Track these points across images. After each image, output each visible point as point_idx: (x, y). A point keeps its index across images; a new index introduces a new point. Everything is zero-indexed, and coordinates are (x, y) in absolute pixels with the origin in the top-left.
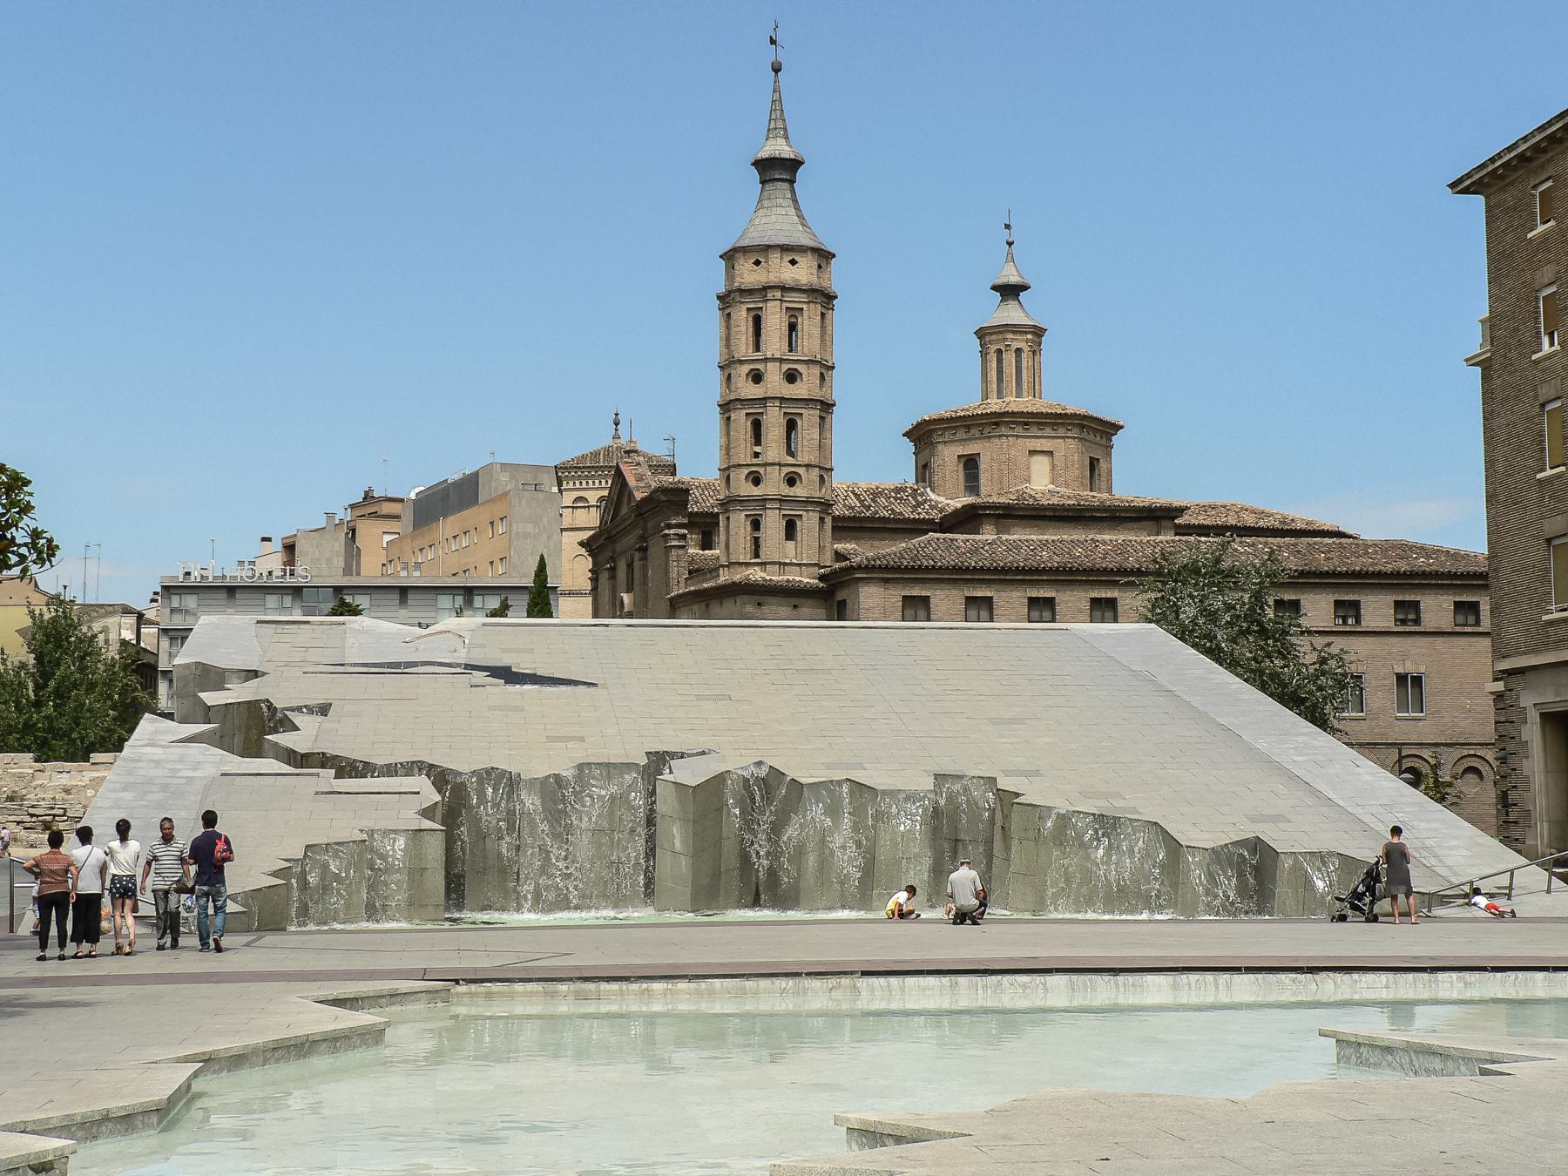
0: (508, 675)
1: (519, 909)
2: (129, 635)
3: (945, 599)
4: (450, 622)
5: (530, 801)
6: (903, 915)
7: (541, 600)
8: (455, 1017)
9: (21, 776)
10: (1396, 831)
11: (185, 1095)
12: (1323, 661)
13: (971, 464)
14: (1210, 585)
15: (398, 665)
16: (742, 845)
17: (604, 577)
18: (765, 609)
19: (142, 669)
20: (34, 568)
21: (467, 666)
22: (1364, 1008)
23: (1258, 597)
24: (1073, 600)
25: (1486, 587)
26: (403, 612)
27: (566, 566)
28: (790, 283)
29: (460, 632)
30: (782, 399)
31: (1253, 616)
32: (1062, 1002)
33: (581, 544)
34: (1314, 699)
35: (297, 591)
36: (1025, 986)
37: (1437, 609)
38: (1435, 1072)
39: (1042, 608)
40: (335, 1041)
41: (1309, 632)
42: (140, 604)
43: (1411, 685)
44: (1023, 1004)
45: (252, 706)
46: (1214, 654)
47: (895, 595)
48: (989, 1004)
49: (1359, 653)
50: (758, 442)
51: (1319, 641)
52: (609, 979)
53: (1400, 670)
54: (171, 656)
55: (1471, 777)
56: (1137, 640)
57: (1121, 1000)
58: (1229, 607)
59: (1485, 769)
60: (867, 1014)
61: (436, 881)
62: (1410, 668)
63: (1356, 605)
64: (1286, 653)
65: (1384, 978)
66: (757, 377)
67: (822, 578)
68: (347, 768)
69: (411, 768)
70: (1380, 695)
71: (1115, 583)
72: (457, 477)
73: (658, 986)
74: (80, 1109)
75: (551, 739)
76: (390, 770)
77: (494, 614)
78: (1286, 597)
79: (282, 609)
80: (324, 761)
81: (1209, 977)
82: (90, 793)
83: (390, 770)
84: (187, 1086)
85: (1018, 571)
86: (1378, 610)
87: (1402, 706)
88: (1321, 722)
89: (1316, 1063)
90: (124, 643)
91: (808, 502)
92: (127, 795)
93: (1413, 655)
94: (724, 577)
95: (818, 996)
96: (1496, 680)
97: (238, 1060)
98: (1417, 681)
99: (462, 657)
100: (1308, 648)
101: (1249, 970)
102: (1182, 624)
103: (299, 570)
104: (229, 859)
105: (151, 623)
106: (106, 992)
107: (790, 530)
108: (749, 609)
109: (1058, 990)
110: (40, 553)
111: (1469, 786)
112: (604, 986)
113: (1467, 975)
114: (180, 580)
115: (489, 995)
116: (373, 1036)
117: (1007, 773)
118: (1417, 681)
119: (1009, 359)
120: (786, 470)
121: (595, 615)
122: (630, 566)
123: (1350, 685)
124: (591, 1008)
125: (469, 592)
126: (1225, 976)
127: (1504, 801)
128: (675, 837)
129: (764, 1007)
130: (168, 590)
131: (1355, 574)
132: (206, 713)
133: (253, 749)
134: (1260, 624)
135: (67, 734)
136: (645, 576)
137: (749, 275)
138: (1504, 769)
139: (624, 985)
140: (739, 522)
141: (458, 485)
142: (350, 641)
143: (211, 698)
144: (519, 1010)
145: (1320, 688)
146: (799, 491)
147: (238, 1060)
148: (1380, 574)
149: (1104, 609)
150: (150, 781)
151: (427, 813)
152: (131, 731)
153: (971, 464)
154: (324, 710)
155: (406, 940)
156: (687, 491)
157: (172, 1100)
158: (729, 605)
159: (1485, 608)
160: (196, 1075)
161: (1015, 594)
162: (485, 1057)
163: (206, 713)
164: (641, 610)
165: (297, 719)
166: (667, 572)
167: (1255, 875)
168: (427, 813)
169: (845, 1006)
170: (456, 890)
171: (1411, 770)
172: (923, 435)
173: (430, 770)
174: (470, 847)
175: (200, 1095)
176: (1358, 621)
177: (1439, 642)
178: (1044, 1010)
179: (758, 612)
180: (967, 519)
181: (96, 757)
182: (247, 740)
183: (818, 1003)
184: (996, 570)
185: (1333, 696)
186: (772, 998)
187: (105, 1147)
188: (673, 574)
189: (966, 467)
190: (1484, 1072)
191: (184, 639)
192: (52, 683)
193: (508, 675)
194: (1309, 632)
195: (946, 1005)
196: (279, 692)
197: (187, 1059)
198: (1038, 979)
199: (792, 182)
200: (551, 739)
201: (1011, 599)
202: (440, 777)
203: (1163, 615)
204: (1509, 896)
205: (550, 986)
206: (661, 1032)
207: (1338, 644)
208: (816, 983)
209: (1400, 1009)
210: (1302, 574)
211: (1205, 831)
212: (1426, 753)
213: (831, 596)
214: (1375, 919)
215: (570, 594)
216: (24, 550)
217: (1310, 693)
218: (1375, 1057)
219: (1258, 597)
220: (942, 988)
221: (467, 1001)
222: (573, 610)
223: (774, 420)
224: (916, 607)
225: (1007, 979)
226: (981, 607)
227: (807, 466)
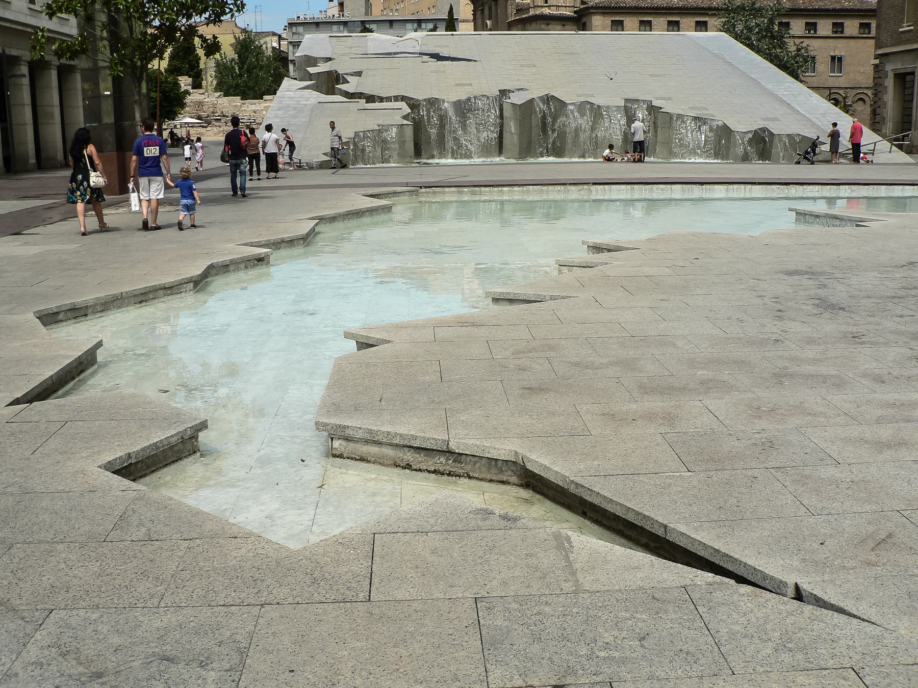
0: (437, 57)
1: (445, 157)
2: (275, 45)
3: (630, 22)
4: (413, 35)
6: (608, 159)
7: (451, 24)
8: (421, 202)
9: (236, 106)
10: (835, 125)
11: (312, 233)
12: (799, 50)
14: (750, 15)
15: (390, 54)
16: (539, 128)
17: (479, 13)
18: (550, 26)
19: (281, 59)
20: (236, 14)
21: (420, 54)
22: (815, 200)
23: (771, 21)
24: (687, 22)
25: (874, 16)
26: (391, 31)
27: (462, 8)
29: (416, 39)
31: (768, 29)
32: (678, 196)
34: (794, 66)
35: (345, 23)
36: (662, 190)
37: (851, 26)
38: (837, 226)
39: (674, 26)
40: (372, 211)
41: (794, 37)
42: (280, 31)
43: (837, 61)
44: (662, 197)
45: (329, 73)
46: (751, 46)
47: (608, 20)
48: (689, 197)
49: (815, 46)
51: (798, 41)
52: (485, 186)
53: (833, 54)
54: (294, 53)
55: (860, 103)
56: (716, 39)
57: (704, 196)
58: (758, 25)
59: (867, 99)
60: (594, 201)
61: (410, 146)
62: (837, 53)
63: (815, 24)
64: (782, 46)
65: (817, 187)
67: (575, 12)
68: (370, 99)
69: (396, 98)
70: (823, 66)
71: (707, 14)
73: (505, 189)
74: (273, 238)
75: (456, 85)
76: (389, 99)
77: (431, 30)
78: (784, 21)
79: (339, 31)
80: (360, 95)
81: (742, 186)
82: (264, 112)
83: (389, 99)
84: (313, 229)
85: (663, 8)
86: (825, 27)
87: (833, 71)
88: (796, 77)
89: (786, 222)
90: (273, 48)
92: (280, 112)
93: (839, 48)
94: (532, 12)
95: (574, 193)
96: (875, 58)
97: (333, 219)
98: (840, 59)
99: (418, 50)
100: (792, 44)
101: (760, 184)
102: (736, 33)
103: (346, 14)
104: (651, 102)
105: (284, 39)
106: (278, 192)
108: (543, 26)
109: (677, 191)
110: (238, 7)
111: (859, 107)
112: (483, 189)
113: (853, 187)
114: (296, 21)
115: (434, 193)
116: (387, 209)
117: (657, 99)
118: (840, 59)
121: (475, 30)
122: (490, 8)
123: (810, 61)
124: (477, 198)
125: (419, 22)
126: (749, 186)
127: (874, 113)
128: (512, 127)
129: (551, 197)
130: (291, 25)
131: (816, 10)
132: (310, 77)
133: (331, 91)
134: (771, 33)
135: (253, 88)
136: (497, 15)
138: (876, 99)
139: (491, 188)
142: (369, 44)
143: (312, 70)
144: (447, 199)
145: (797, 62)
147: (333, 219)
148: (827, 10)
149: (702, 26)
150: (288, 106)
152: (279, 86)
154: (359, 74)
155: (397, 171)
157: (308, 234)
158: (534, 25)
159: (874, 26)
160: (316, 224)
161: (662, 19)
162: (433, 218)
163: (310, 77)
164: (495, 28)
165: (349, 78)
166: (506, 10)
167: (762, 144)
168: (405, 117)
169: (585, 198)
170: (418, 153)
171: (833, 99)
173: (403, 98)
174: (426, 132)
175: (318, 233)
176: (815, 32)
177: (852, 42)
178: (671, 200)
179: (547, 28)
181: (266, 97)
182: (328, 88)
183: (573, 196)
184: (653, 8)
185: (802, 66)
186: (555, 194)
187: (284, 252)
188: (509, 12)
190: (857, 226)
191: (299, 46)
192: (245, 67)
193: (437, 57)
194: (794, 37)
195: (629, 197)
196: (341, 67)
197: (312, 219)
198: (669, 186)
200: (456, 85)
201: (660, 22)
202: (414, 105)
203: (728, 29)
204: (873, 154)
205: (460, 189)
206: (507, 207)
207: (806, 42)
208: (573, 188)
209: (831, 201)
210: (792, 10)
211: (743, 124)
212: (841, 92)
214: (813, 163)
215: (464, 21)
216: (231, 6)
217: (792, 64)
218: (811, 219)
219: (771, 21)
220: (627, 190)
221: (426, 196)
222: (465, 28)
224: (618, 25)
225: (655, 186)
226: (646, 25)
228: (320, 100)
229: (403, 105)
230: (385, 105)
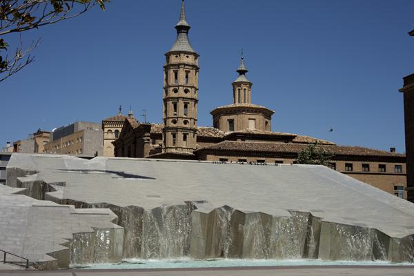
5: (223, 209)
13: (231, 122)
28: (186, 63)
30: (183, 98)
33: (112, 143)
45: (36, 183)
50: (175, 111)
66: (176, 91)
67: (194, 152)
68: (79, 205)
72: (67, 125)
80: (68, 202)
91: (190, 129)
107: (185, 138)
117: (314, 211)
119: (242, 91)
120: (184, 119)
137: (173, 60)
140: (169, 135)
141: (68, 128)
146: (188, 126)
150: (6, 208)
151: (114, 221)
153: (231, 122)
154: (62, 184)
156: (151, 126)
163: (20, 185)
165: (56, 187)
168: (114, 221)
172: (217, 114)
173: (111, 207)
180: (233, 137)
189: (230, 123)
199: (187, 33)
213: (199, 156)
223: (181, 104)
227: (190, 119)
228: (35, 204)
229: (108, 211)
230: (94, 210)
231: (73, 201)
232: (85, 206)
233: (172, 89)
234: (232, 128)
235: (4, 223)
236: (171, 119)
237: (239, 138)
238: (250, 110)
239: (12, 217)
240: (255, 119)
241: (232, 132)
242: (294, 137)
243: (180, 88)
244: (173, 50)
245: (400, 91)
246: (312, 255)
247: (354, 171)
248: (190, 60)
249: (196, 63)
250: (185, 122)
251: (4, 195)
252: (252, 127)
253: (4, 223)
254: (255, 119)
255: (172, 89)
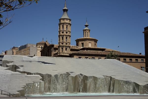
5: (80, 75)
13: (83, 44)
28: (67, 23)
30: (66, 35)
33: (40, 51)
45: (13, 66)
50: (63, 40)
66: (63, 33)
67: (69, 55)
68: (28, 73)
72: (24, 45)
80: (24, 72)
91: (68, 46)
107: (66, 50)
117: (112, 76)
119: (87, 33)
120: (66, 43)
137: (62, 21)
140: (61, 48)
141: (24, 46)
146: (67, 45)
150: (2, 74)
151: (41, 79)
153: (83, 44)
154: (22, 66)
156: (54, 45)
163: (7, 66)
165: (20, 67)
168: (41, 79)
172: (78, 41)
173: (40, 74)
180: (83, 49)
189: (82, 44)
199: (67, 12)
213: (71, 56)
223: (65, 37)
227: (68, 43)
228: (12, 73)
229: (39, 76)
230: (34, 75)
231: (26, 72)
232: (30, 74)
233: (61, 32)
234: (83, 46)
235: (1, 80)
236: (61, 43)
237: (86, 49)
238: (89, 40)
239: (4, 78)
240: (91, 43)
241: (83, 47)
242: (105, 49)
243: (64, 31)
244: (62, 18)
245: (143, 33)
246: (112, 91)
247: (127, 61)
248: (68, 22)
249: (70, 23)
250: (66, 44)
251: (2, 70)
252: (90, 46)
253: (1, 80)
254: (91, 43)
255: (61, 32)
